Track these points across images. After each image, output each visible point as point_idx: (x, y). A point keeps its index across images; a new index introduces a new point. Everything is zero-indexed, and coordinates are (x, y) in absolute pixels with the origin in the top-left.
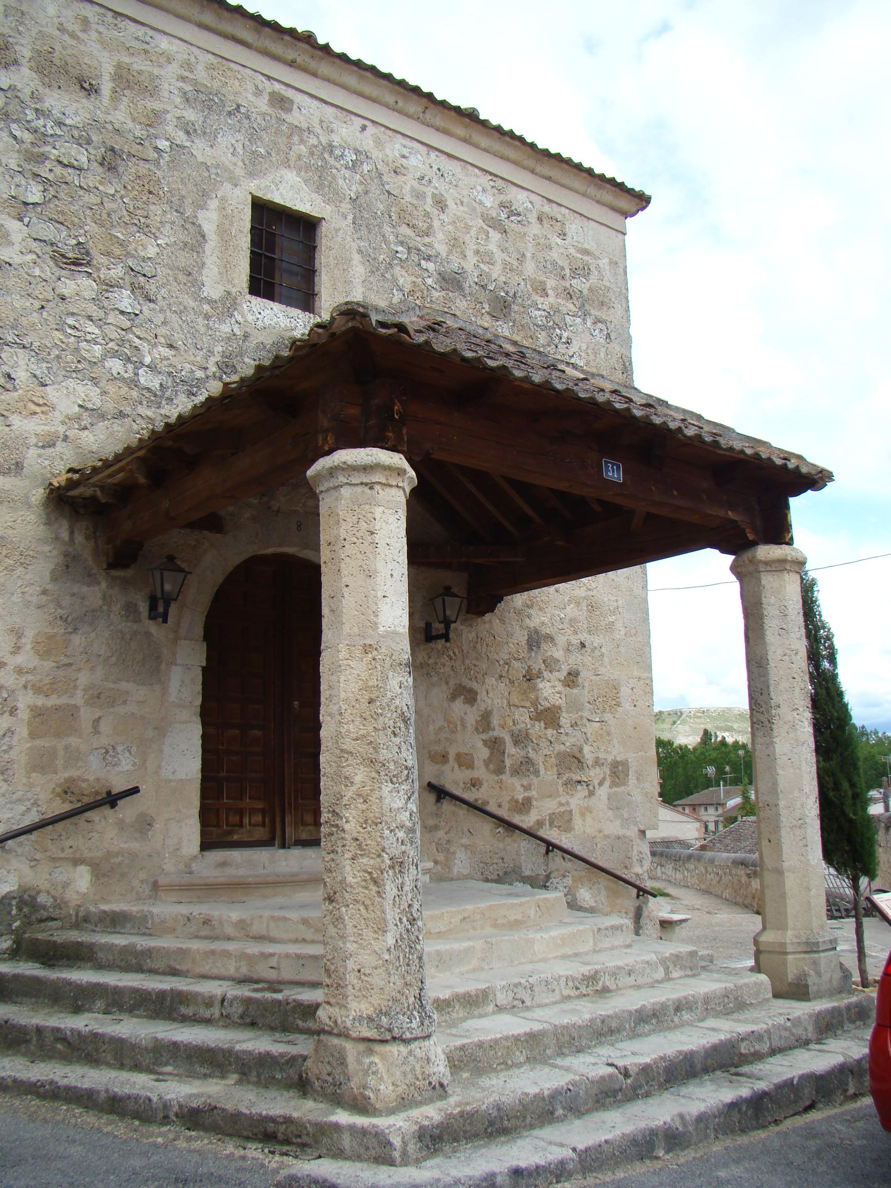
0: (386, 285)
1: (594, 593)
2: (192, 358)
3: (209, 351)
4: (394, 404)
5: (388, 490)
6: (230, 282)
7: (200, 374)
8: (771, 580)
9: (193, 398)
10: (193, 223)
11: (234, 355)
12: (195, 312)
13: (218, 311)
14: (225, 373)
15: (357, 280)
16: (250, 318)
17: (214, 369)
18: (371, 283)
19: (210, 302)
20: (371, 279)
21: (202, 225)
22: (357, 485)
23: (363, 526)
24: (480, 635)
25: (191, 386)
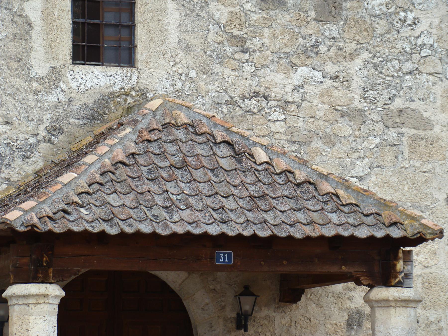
0: (201, 24)
1: (433, 269)
2: (25, 129)
3: (39, 120)
4: (44, 257)
5: (38, 306)
6: (55, 58)
7: (32, 140)
8: (382, 313)
9: (27, 160)
10: (21, 16)
11: (60, 118)
12: (26, 91)
13: (45, 86)
14: (54, 135)
15: (172, 27)
16: (74, 85)
17: (44, 134)
18: (186, 26)
19: (38, 79)
20: (186, 22)
21: (28, 15)
22: (21, 304)
23: (24, 326)
24: (294, 319)
25: (25, 151)
